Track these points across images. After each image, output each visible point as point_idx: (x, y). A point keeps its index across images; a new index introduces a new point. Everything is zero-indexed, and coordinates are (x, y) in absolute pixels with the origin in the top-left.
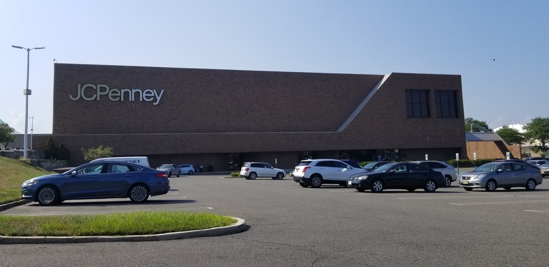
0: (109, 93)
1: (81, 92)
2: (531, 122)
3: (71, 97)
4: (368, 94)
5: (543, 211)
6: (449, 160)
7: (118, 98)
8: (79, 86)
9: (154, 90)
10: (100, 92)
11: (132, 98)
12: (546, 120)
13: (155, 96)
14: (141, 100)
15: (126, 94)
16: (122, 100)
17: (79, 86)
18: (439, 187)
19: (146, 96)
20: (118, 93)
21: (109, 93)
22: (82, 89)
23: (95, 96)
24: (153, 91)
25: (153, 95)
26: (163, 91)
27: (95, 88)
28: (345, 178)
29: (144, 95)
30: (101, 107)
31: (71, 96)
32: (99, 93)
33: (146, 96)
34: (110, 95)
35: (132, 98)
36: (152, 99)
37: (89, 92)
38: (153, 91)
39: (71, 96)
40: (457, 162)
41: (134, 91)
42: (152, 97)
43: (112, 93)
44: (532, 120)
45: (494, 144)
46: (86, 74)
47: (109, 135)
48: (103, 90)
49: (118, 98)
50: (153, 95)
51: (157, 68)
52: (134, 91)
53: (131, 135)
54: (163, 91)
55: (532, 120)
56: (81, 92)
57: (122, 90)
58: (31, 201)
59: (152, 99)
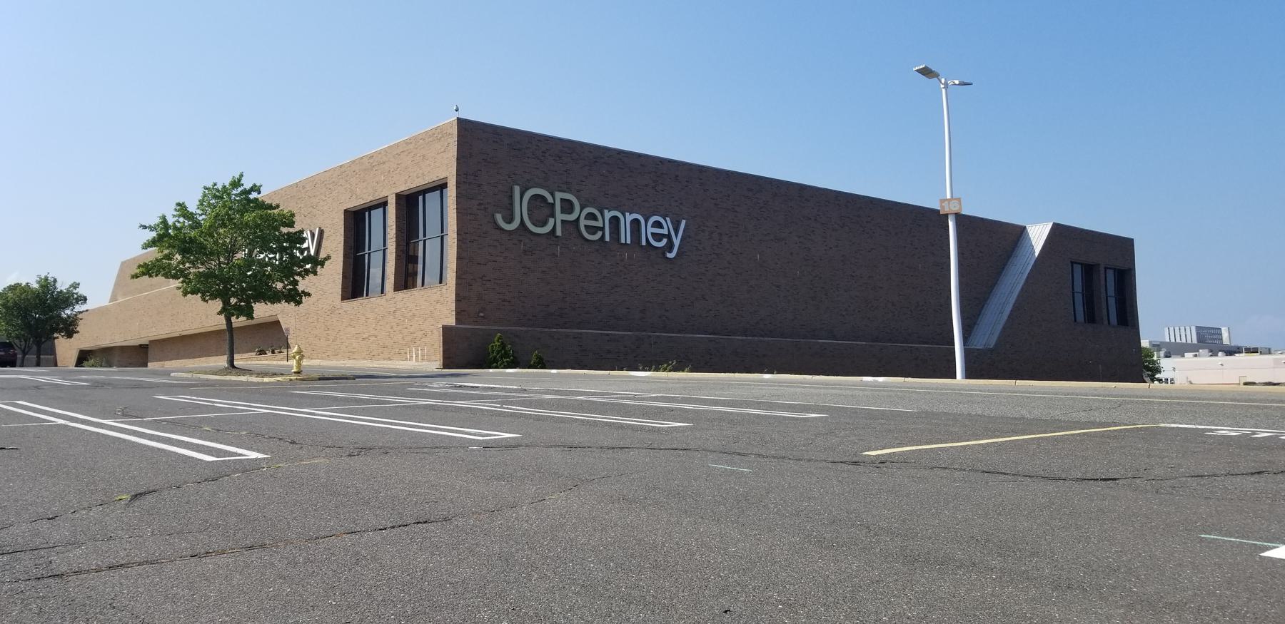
0: (580, 215)
1: (521, 209)
2: (269, 304)
3: (501, 219)
4: (1009, 257)
7: (599, 234)
8: (517, 190)
9: (668, 219)
10: (652, 227)
11: (626, 237)
12: (276, 221)
13: (669, 236)
14: (644, 243)
15: (615, 221)
16: (607, 238)
17: (517, 190)
19: (586, 226)
21: (580, 215)
22: (583, 212)
23: (551, 221)
24: (666, 221)
26: (684, 222)
27: (550, 200)
28: (1249, 357)
30: (561, 253)
31: (499, 217)
32: (560, 216)
33: (586, 226)
34: (583, 222)
35: (626, 237)
37: (541, 208)
38: (666, 221)
39: (499, 217)
41: (630, 217)
44: (241, 175)
46: (528, 157)
47: (607, 335)
48: (568, 207)
49: (599, 234)
50: (665, 231)
51: (640, 156)
52: (630, 217)
53: (650, 336)
54: (684, 222)
55: (241, 175)
56: (521, 209)
57: (606, 211)
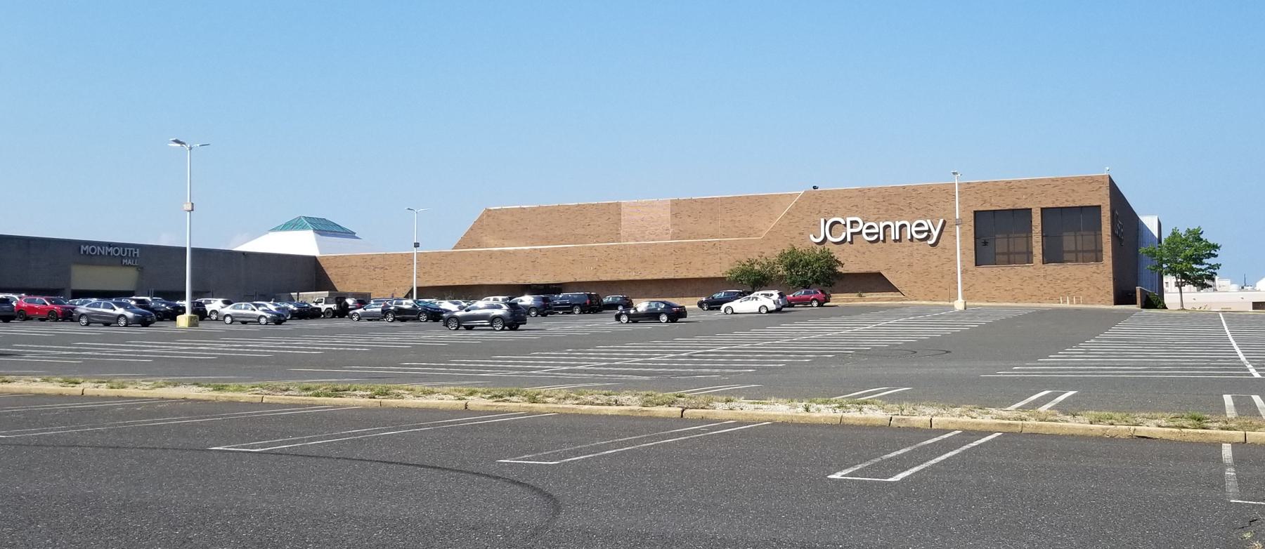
1: (824, 230)
5: (392, 370)
6: (522, 295)
7: (876, 236)
11: (894, 234)
13: (929, 231)
18: (1256, 282)
20: (923, 225)
25: (927, 229)
29: (914, 229)
31: (811, 236)
34: (864, 231)
36: (926, 234)
39: (811, 236)
40: (193, 315)
42: (925, 231)
43: (868, 228)
45: (328, 268)
49: (876, 236)
50: (926, 228)
52: (898, 224)
58: (978, 437)
59: (926, 234)
